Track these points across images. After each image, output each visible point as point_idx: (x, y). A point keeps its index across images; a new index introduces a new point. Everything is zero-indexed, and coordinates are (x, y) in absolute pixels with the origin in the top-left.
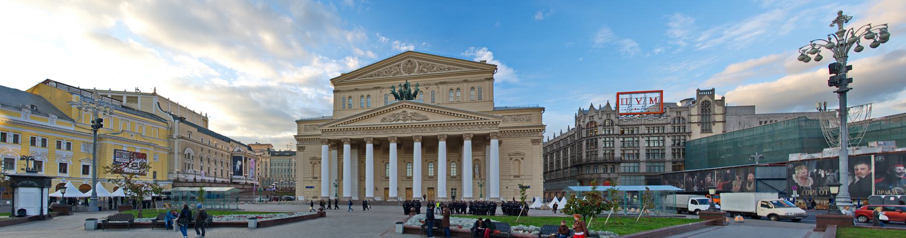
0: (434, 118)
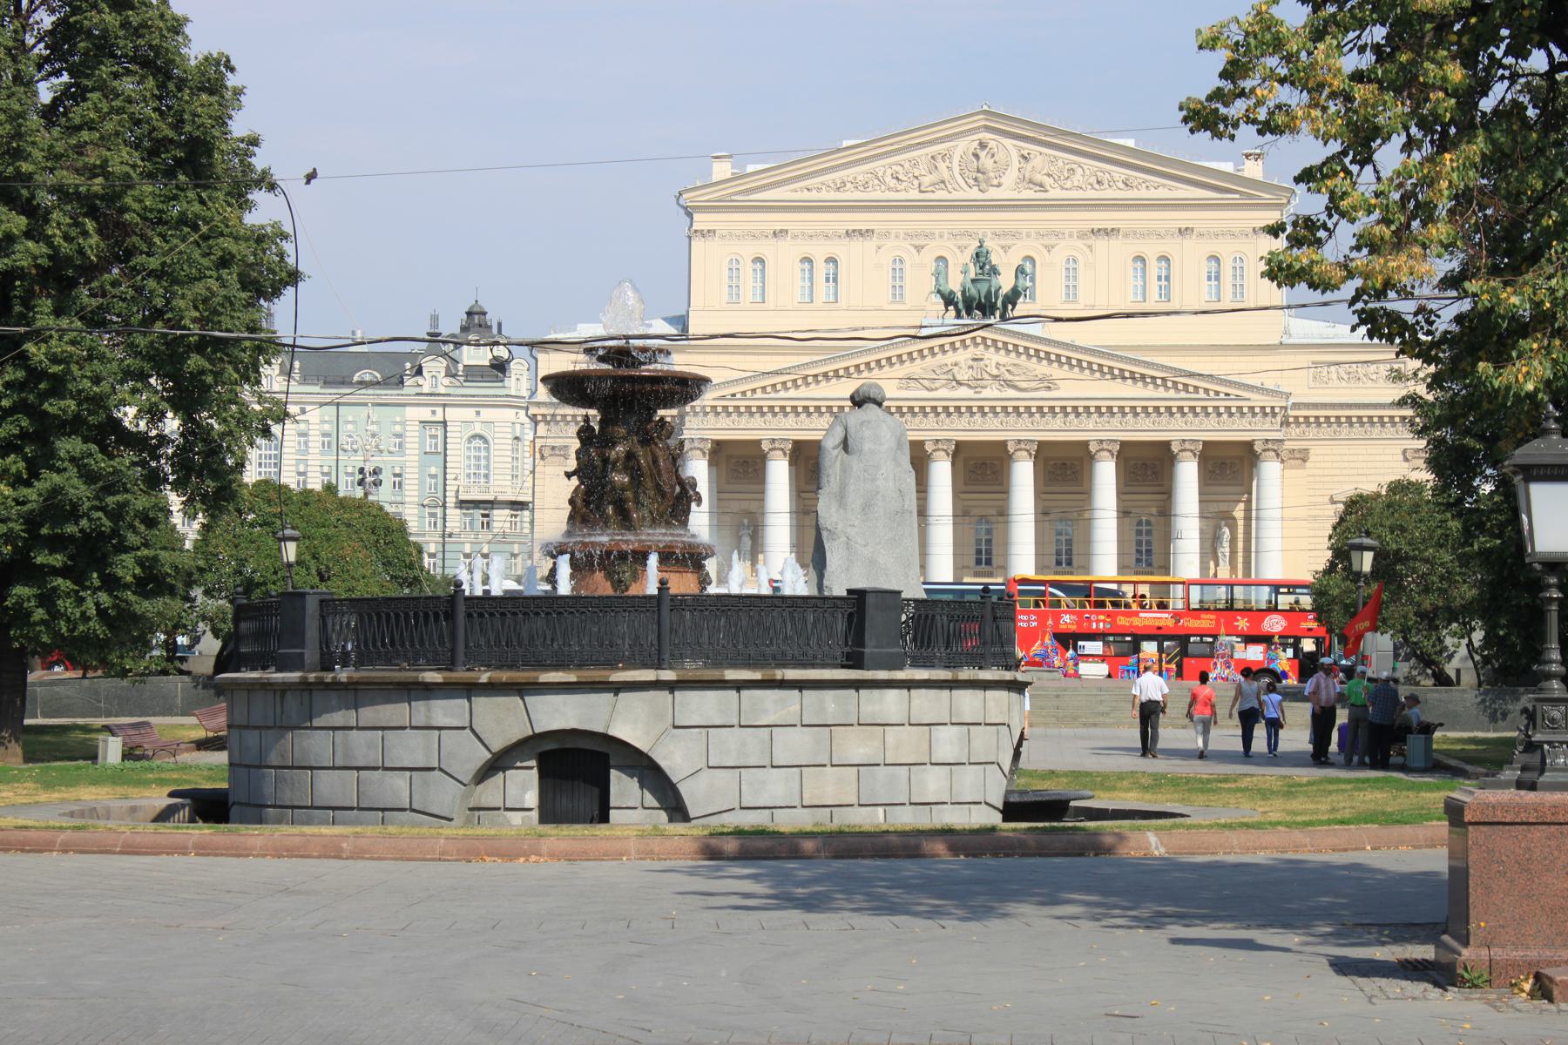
0: (1075, 387)
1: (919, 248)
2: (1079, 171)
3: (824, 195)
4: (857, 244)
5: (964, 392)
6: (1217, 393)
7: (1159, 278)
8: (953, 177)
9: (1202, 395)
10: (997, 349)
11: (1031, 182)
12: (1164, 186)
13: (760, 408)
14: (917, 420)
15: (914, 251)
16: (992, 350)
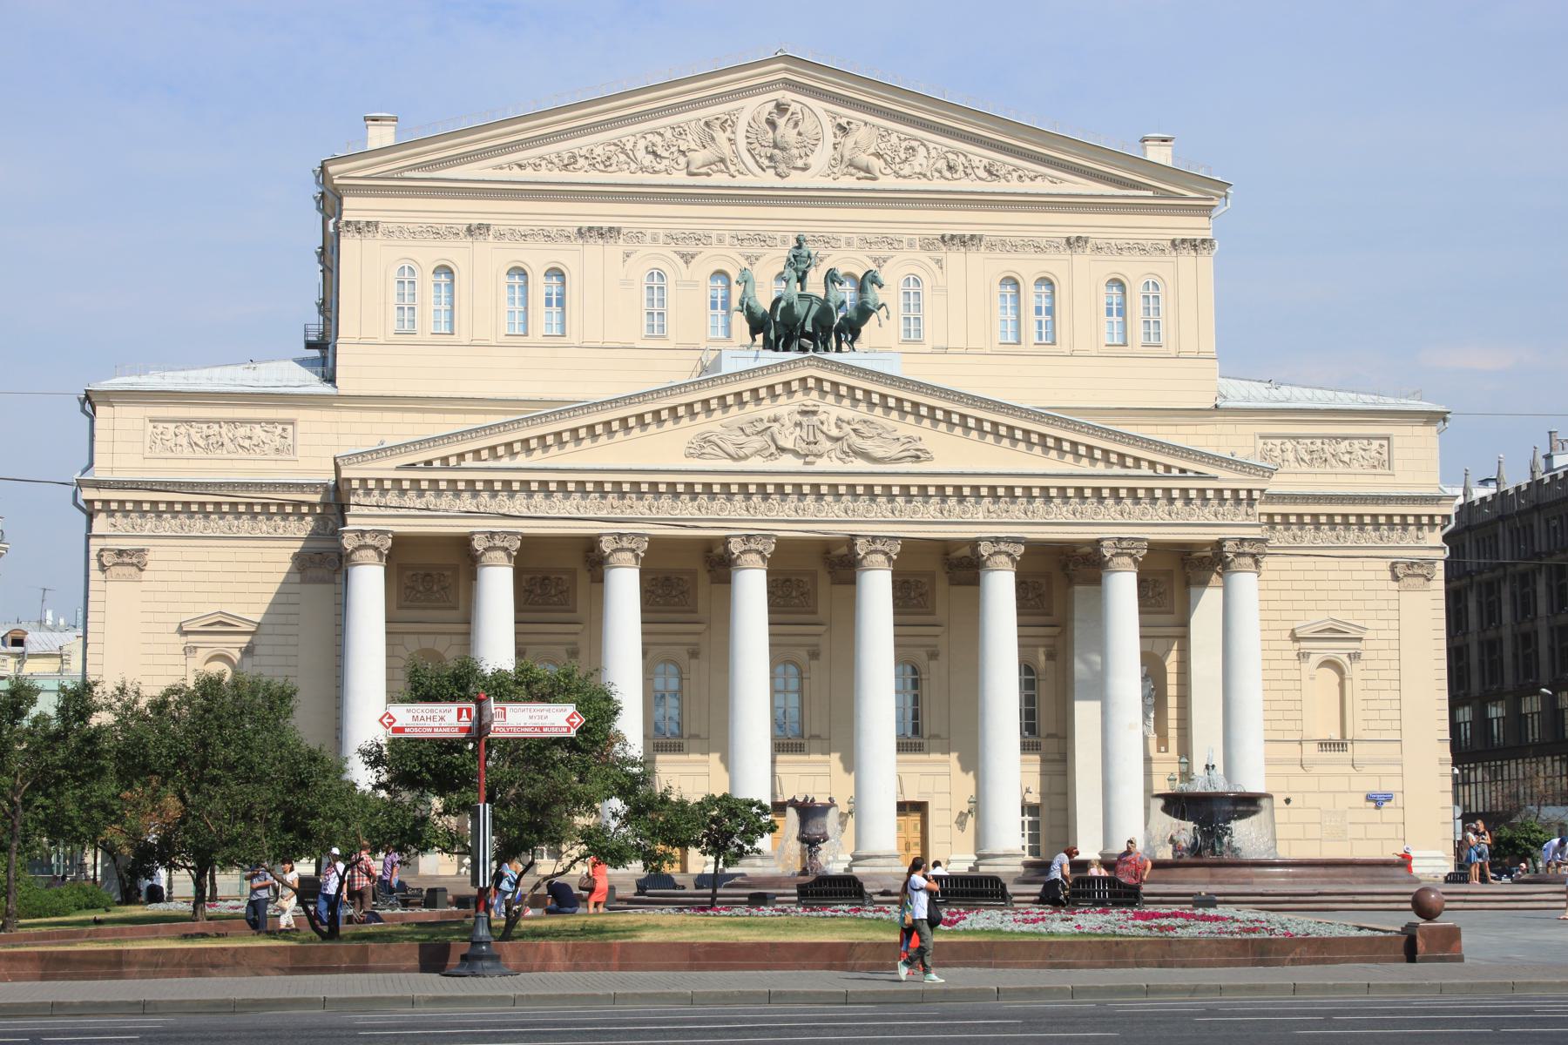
0: (954, 454)
1: (687, 258)
2: (922, 151)
3: (544, 174)
4: (594, 250)
5: (788, 462)
6: (1168, 468)
7: (1038, 311)
8: (737, 154)
9: (1145, 470)
10: (839, 397)
11: (851, 164)
12: (1043, 176)
13: (471, 483)
14: (716, 505)
15: (680, 262)
16: (831, 398)
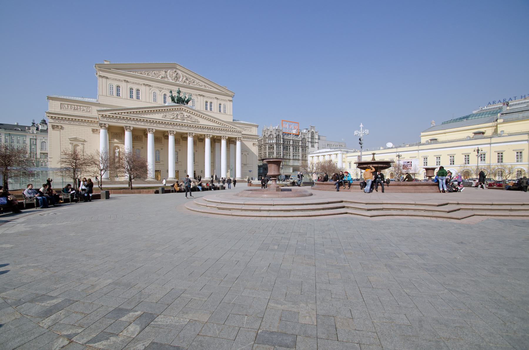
0: (203, 122)
9: (123, 114)
